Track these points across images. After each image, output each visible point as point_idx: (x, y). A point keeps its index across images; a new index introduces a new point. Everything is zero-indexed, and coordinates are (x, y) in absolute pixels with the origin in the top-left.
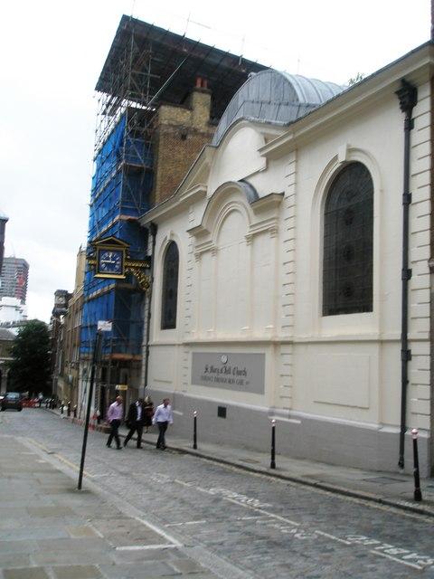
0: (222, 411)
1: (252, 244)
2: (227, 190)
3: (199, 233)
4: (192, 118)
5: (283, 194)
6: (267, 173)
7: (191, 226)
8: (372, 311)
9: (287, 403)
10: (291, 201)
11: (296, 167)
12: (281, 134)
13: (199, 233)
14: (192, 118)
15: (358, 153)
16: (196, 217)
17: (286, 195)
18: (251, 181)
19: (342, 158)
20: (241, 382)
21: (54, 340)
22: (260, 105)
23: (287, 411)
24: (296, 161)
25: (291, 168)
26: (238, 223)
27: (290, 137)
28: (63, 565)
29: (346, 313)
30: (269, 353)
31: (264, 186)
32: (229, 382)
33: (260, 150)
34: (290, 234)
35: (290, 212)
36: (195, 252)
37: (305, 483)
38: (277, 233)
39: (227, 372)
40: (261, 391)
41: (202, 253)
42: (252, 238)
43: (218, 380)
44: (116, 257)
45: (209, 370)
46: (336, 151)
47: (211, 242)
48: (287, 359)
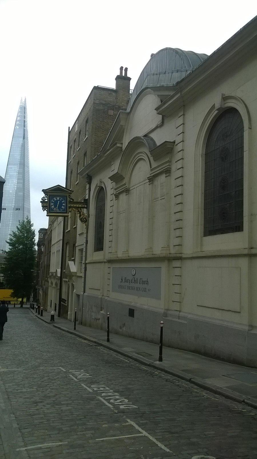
0: (131, 312)
1: (152, 183)
2: (136, 143)
3: (117, 178)
4: (116, 98)
5: (174, 142)
6: (163, 128)
7: (112, 174)
8: (242, 230)
9: (176, 306)
10: (179, 147)
11: (184, 120)
12: (171, 93)
13: (117, 178)
14: (116, 98)
15: (233, 101)
16: (115, 167)
17: (176, 143)
18: (152, 135)
19: (217, 106)
20: (145, 290)
21: (38, 262)
22: (158, 75)
23: (178, 313)
24: (184, 115)
25: (180, 121)
26: (142, 170)
27: (179, 95)
28: (169, 375)
29: (222, 233)
30: (164, 266)
31: (159, 138)
32: (137, 289)
33: (157, 109)
34: (179, 173)
35: (179, 156)
36: (115, 193)
37: (183, 378)
38: (129, 192)
39: (135, 281)
40: (158, 297)
41: (120, 193)
42: (151, 179)
43: (129, 288)
44: (54, 200)
45: (124, 281)
46: (212, 101)
47: (125, 184)
48: (177, 272)
